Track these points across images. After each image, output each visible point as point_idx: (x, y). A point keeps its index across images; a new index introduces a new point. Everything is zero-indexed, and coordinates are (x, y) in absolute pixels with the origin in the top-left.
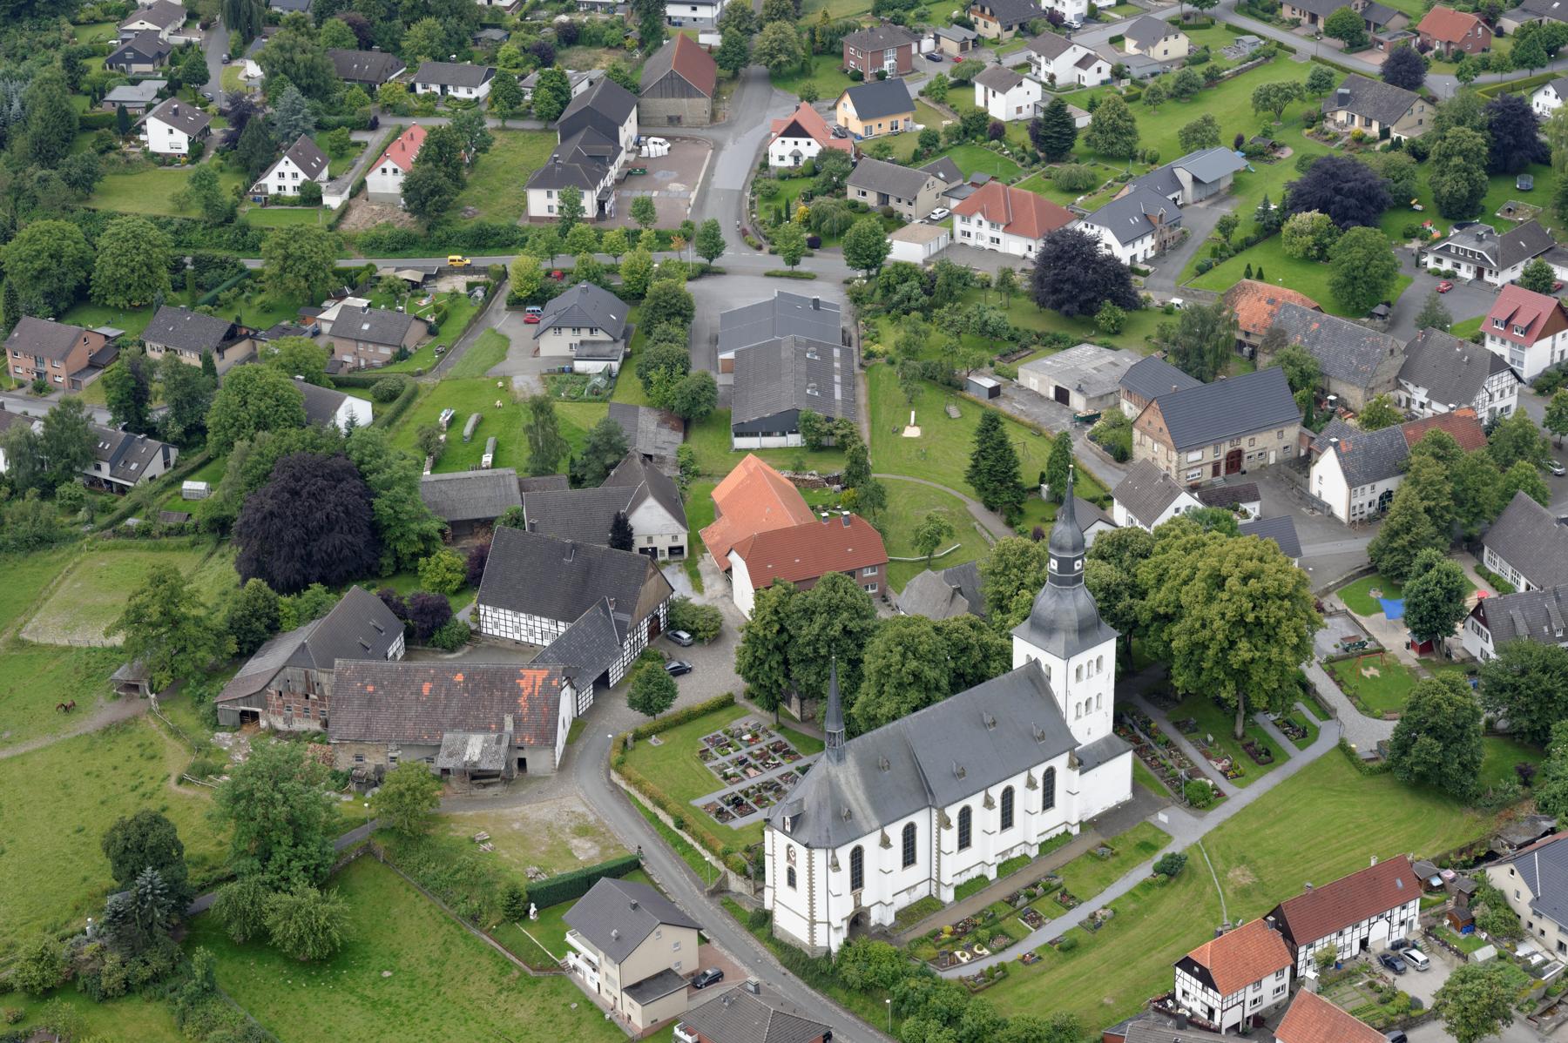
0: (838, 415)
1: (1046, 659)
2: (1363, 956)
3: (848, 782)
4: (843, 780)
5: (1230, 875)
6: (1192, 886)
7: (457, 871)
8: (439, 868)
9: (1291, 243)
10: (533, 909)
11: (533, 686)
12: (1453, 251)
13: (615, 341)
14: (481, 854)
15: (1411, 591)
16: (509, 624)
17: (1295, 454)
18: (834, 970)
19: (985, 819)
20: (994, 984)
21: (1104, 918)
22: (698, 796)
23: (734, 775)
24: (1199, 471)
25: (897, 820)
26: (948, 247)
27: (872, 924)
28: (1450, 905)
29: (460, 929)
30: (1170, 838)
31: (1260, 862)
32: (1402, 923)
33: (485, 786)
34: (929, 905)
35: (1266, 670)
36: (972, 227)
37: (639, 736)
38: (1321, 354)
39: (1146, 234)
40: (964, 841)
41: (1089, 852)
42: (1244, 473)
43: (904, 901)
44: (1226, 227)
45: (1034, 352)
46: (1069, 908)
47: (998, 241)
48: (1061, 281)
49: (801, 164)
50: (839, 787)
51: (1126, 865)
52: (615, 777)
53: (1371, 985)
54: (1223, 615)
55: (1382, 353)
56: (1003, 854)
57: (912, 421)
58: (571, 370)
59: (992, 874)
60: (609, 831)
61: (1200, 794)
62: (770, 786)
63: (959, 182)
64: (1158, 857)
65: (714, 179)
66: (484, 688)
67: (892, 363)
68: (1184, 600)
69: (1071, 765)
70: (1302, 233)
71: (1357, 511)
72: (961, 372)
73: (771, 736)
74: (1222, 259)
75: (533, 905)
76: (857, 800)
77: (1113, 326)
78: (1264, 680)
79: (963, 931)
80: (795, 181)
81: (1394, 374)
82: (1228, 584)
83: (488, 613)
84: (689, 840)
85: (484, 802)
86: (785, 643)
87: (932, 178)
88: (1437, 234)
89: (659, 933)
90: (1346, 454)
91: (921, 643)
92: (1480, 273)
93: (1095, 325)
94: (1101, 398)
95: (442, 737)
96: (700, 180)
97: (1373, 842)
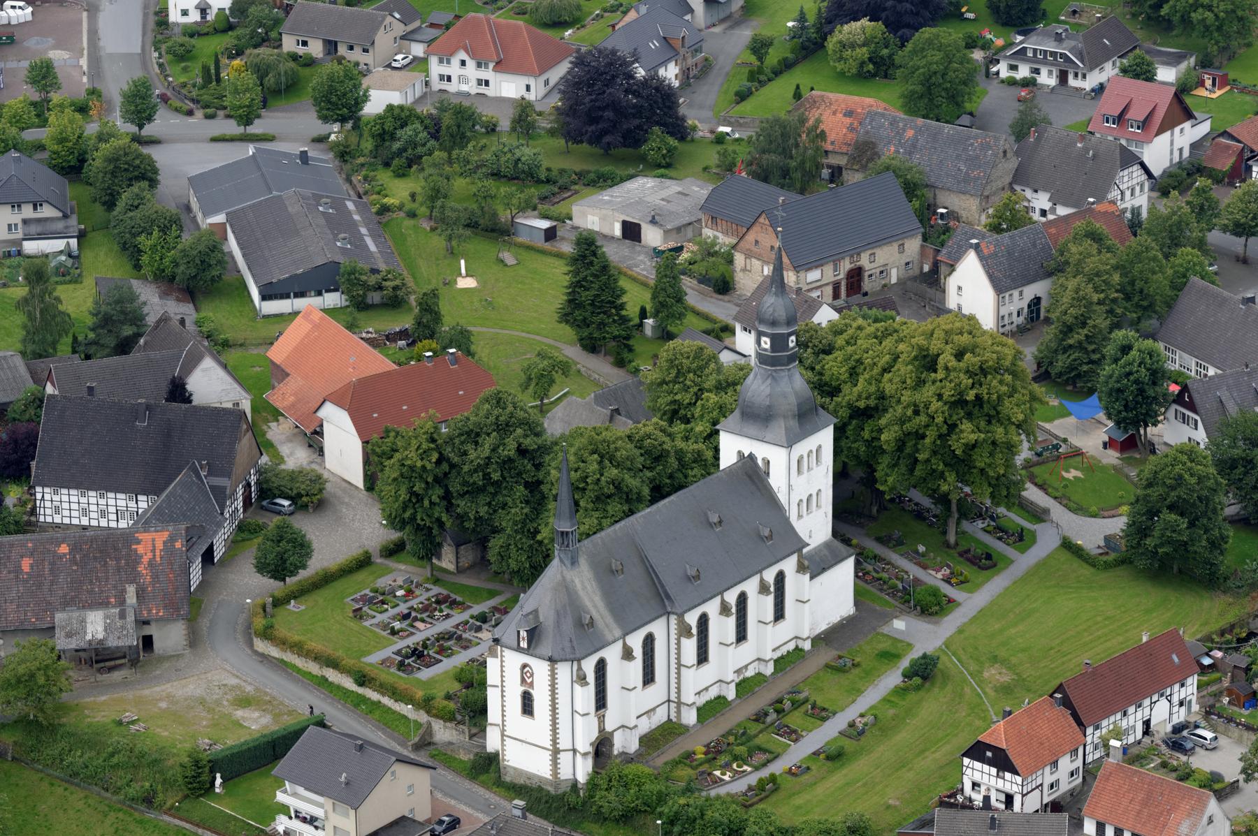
0: (382, 267)
1: (761, 451)
2: (1147, 740)
3: (584, 588)
4: (579, 586)
5: (986, 674)
6: (949, 688)
7: (112, 755)
8: (86, 756)
9: (841, 58)
10: (219, 781)
11: (153, 551)
12: (1030, 54)
13: (65, 216)
14: (134, 735)
15: (1111, 376)
16: (74, 506)
17: (917, 272)
18: (584, 803)
19: (722, 628)
20: (767, 797)
21: (865, 724)
22: (369, 653)
23: (402, 630)
24: (819, 293)
25: (635, 630)
26: (423, 97)
27: (616, 752)
28: (1226, 683)
29: (131, 815)
30: (910, 645)
31: (1014, 660)
32: (1181, 704)
33: (111, 669)
34: (669, 731)
35: (991, 454)
36: (454, 69)
37: (278, 602)
38: (922, 163)
39: (669, 60)
40: (703, 657)
41: (827, 666)
42: (866, 294)
43: (645, 726)
44: (759, 47)
45: (576, 192)
46: (824, 719)
47: (487, 83)
48: (599, 108)
49: (209, 18)
50: (576, 593)
51: (871, 675)
52: (261, 645)
53: (1164, 765)
54: (940, 397)
55: (995, 155)
56: (738, 672)
57: (463, 271)
58: (19, 253)
59: (731, 694)
60: (274, 698)
61: (932, 599)
62: (444, 637)
63: (417, 24)
64: (905, 663)
65: (101, 43)
66: (95, 558)
67: (412, 215)
68: (889, 388)
69: (801, 568)
70: (853, 46)
71: (1006, 321)
72: (504, 215)
73: (428, 590)
74: (762, 84)
75: (218, 775)
76: (595, 606)
77: (664, 156)
78: (990, 465)
79: (714, 752)
80: (206, 38)
81: (1008, 179)
82: (941, 360)
83: (47, 497)
84: (374, 696)
85: (113, 686)
86: (446, 474)
87: (389, 18)
88: (1000, 42)
89: (393, 773)
90: (990, 256)
91: (617, 449)
92: (1063, 77)
93: (643, 159)
94: (679, 230)
95: (53, 618)
96: (85, 44)
97: (1127, 631)
